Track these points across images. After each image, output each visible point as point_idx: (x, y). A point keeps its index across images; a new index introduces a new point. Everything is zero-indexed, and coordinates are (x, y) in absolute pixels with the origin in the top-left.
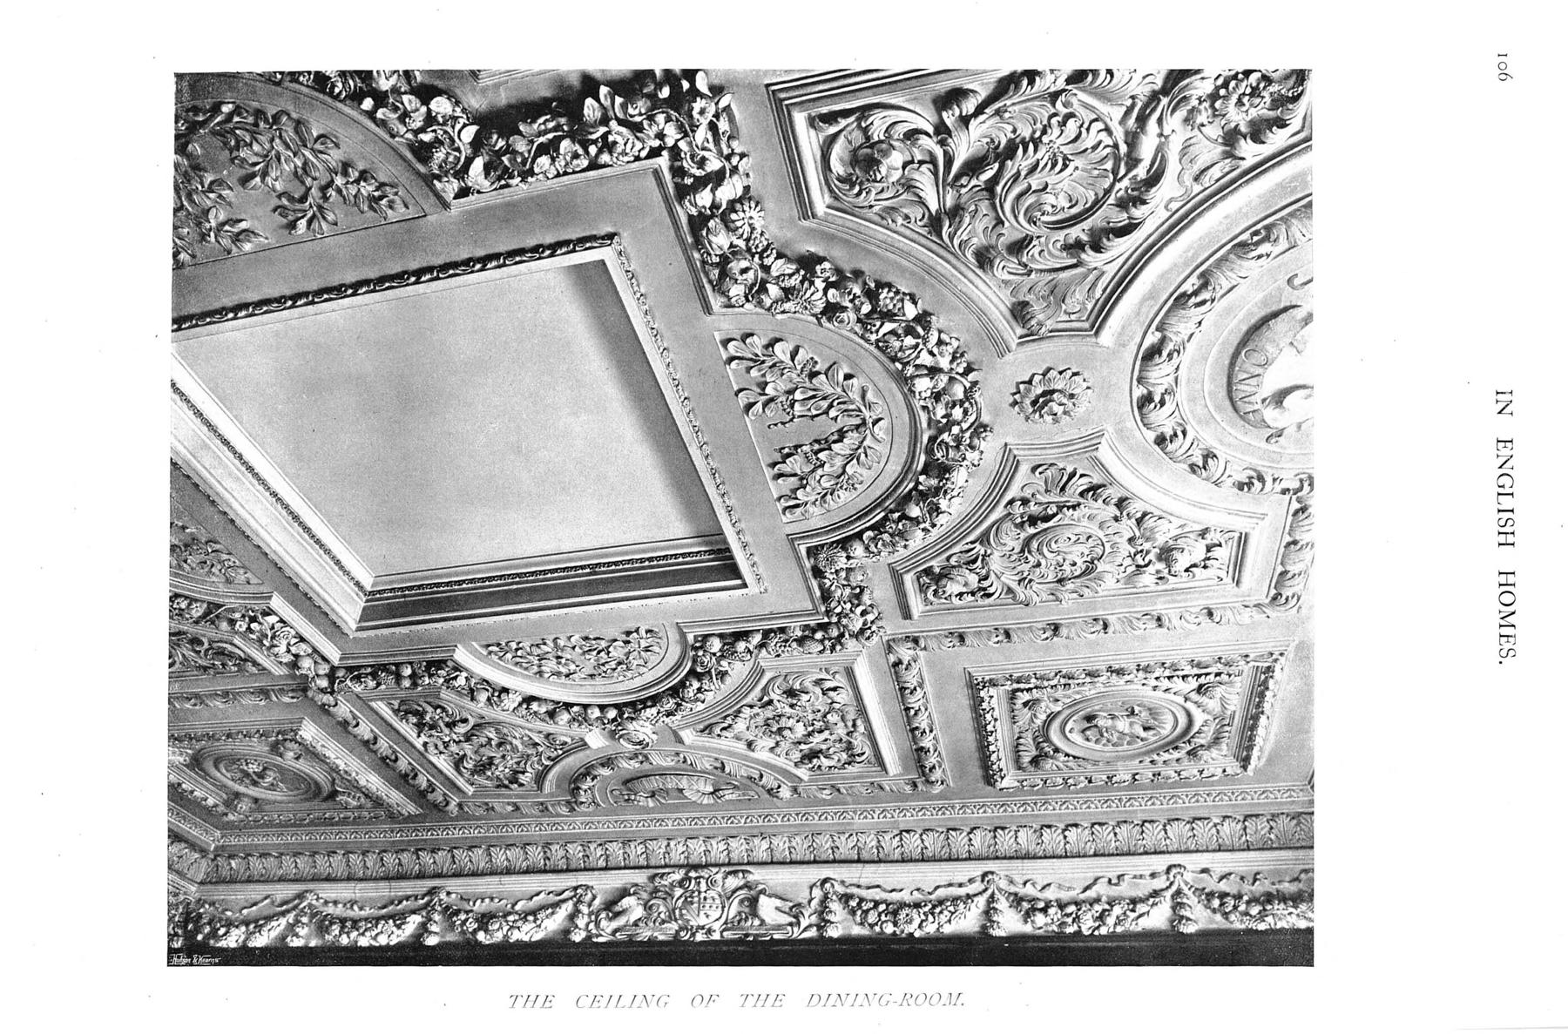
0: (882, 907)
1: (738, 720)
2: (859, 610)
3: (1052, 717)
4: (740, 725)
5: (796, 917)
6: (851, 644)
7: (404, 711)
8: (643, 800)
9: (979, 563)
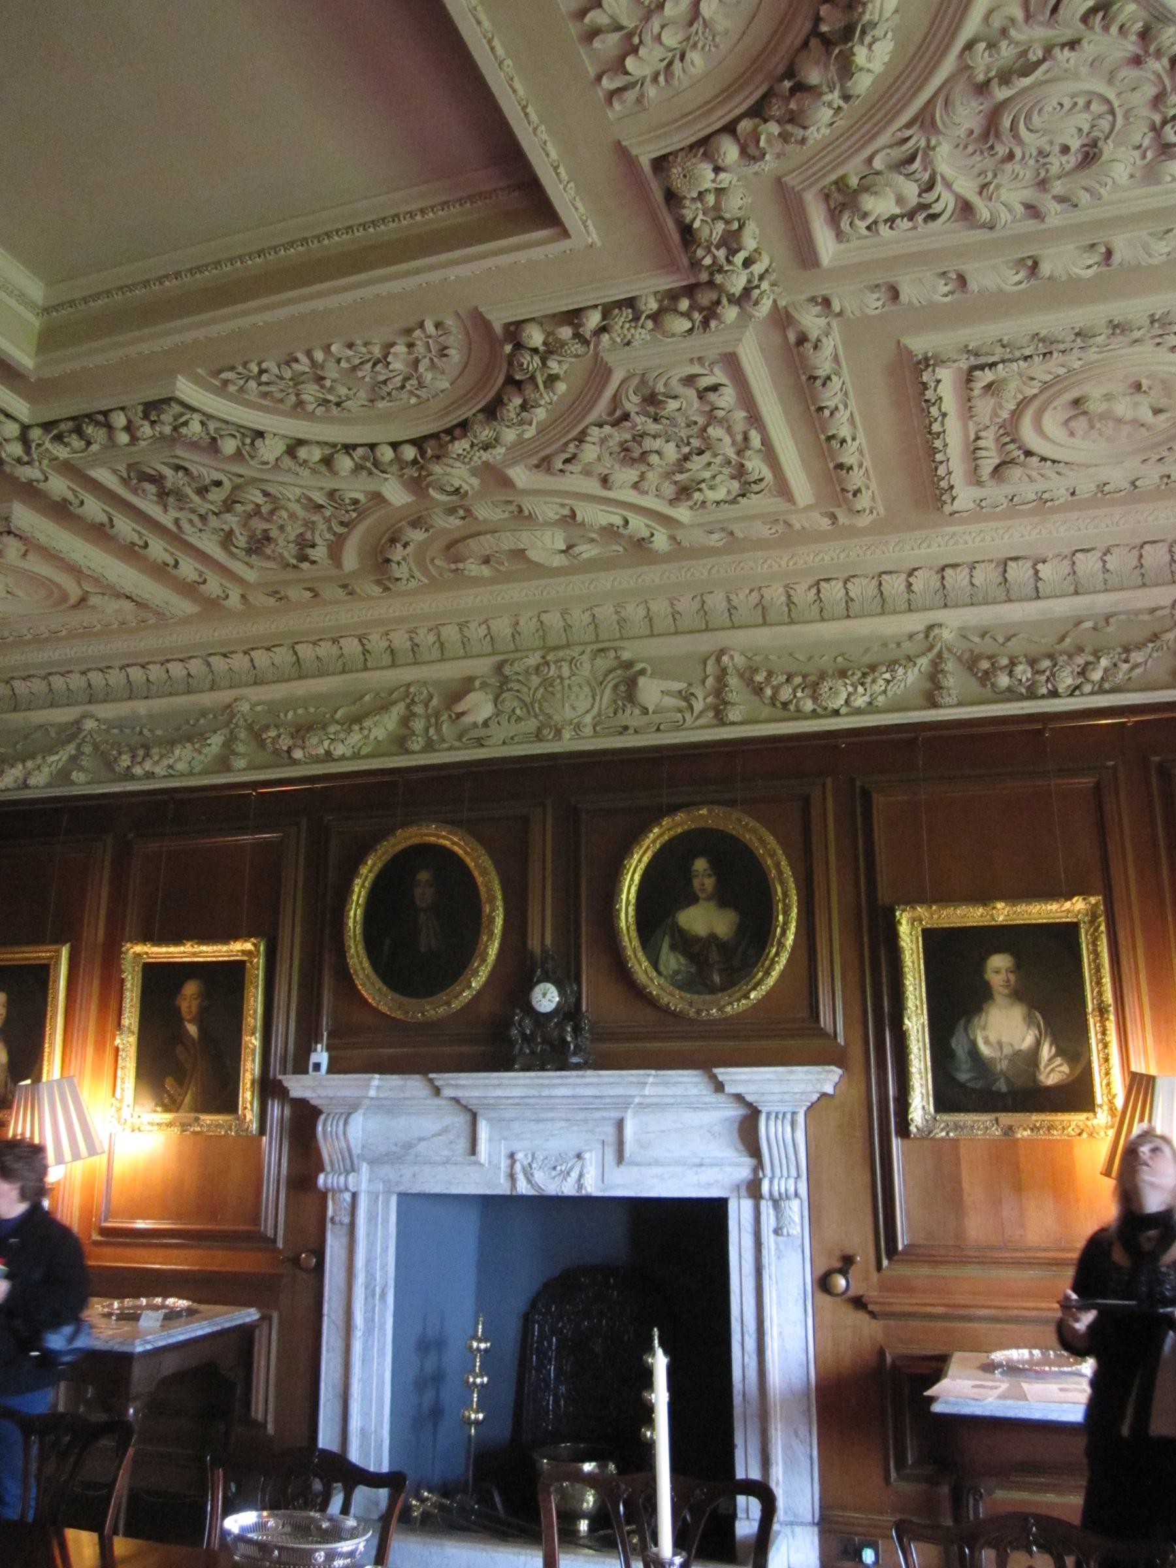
0: (798, 680)
1: (586, 446)
2: (739, 259)
3: (1022, 405)
4: (590, 453)
5: (686, 699)
6: (730, 313)
7: (141, 476)
8: (473, 568)
9: (917, 165)
